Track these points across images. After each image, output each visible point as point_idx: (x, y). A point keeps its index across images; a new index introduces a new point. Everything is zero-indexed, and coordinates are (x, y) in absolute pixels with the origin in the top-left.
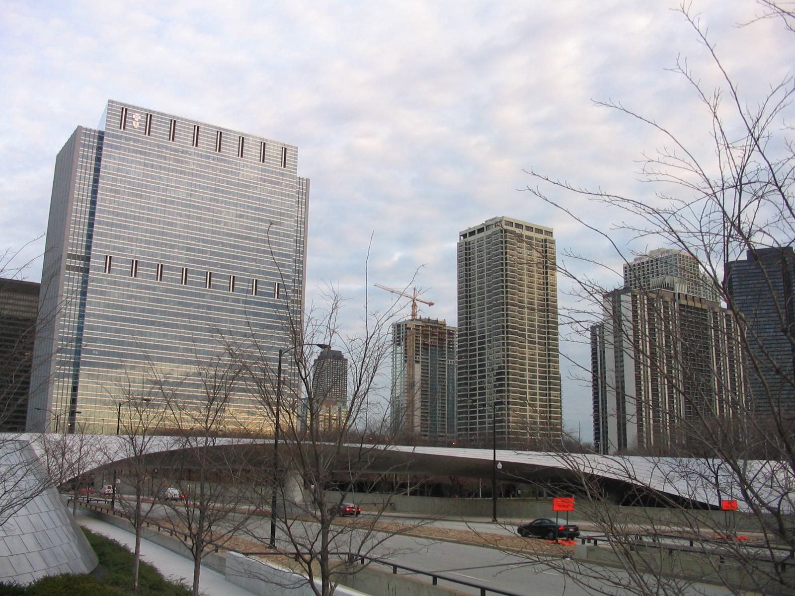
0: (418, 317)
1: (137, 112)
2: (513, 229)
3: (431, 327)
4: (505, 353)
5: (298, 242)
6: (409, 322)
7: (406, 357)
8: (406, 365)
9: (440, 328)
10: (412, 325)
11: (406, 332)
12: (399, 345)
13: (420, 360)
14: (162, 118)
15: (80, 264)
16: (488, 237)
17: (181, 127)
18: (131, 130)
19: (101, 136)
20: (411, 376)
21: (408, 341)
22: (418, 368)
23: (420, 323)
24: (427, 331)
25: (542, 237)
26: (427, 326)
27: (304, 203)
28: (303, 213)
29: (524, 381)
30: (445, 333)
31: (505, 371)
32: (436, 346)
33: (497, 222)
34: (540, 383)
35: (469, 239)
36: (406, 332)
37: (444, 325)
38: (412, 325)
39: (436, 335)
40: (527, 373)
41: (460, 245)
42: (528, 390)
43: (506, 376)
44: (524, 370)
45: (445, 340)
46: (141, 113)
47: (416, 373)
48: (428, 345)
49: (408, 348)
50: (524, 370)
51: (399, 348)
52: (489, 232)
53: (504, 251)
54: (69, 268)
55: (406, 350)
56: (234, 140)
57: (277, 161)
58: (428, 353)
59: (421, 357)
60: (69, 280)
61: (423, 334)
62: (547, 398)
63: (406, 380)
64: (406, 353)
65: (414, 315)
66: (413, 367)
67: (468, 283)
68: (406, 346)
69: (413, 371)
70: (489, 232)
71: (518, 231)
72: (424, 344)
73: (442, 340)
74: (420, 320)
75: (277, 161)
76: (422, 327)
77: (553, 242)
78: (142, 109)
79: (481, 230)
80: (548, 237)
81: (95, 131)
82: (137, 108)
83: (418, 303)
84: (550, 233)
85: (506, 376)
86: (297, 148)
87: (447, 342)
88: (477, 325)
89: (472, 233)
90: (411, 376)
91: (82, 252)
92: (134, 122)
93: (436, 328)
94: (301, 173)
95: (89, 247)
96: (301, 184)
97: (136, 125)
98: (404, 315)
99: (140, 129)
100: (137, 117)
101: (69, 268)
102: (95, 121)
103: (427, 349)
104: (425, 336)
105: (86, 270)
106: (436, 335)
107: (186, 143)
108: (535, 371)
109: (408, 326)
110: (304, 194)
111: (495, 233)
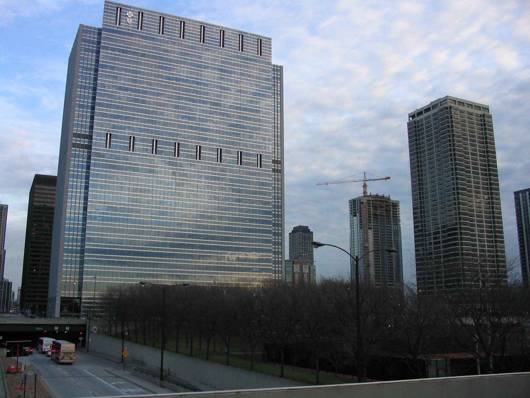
0: (368, 194)
1: (130, 10)
2: (457, 106)
3: (380, 201)
4: (457, 211)
5: (276, 180)
6: (363, 198)
7: (361, 225)
8: (361, 231)
9: (386, 202)
10: (364, 200)
11: (360, 205)
12: (355, 216)
13: (372, 227)
14: (152, 15)
15: (86, 142)
16: (434, 115)
17: (169, 22)
18: (125, 26)
19: (100, 30)
20: (365, 240)
21: (362, 212)
22: (371, 233)
23: (372, 199)
24: (376, 204)
25: (481, 112)
26: (376, 201)
27: (279, 137)
28: (280, 154)
29: (474, 235)
30: (390, 205)
31: (458, 226)
32: (383, 216)
33: (446, 99)
34: (488, 236)
35: (417, 119)
36: (360, 205)
37: (389, 199)
38: (364, 200)
39: (383, 207)
40: (476, 228)
41: (409, 124)
42: (477, 243)
43: (458, 231)
44: (473, 225)
45: (390, 211)
46: (133, 11)
47: (369, 237)
48: (378, 214)
49: (362, 217)
50: (473, 225)
51: (355, 218)
52: (436, 110)
53: (450, 125)
54: (74, 145)
55: (361, 219)
56: (216, 33)
57: (254, 50)
58: (377, 221)
59: (372, 224)
60: (75, 156)
61: (373, 207)
62: (494, 249)
63: (362, 242)
64: (361, 222)
65: (365, 192)
66: (367, 233)
67: (419, 155)
68: (361, 216)
69: (367, 235)
70: (436, 110)
71: (461, 108)
72: (374, 214)
73: (388, 211)
74: (370, 196)
75: (254, 50)
76: (373, 201)
77: (490, 117)
78: (134, 8)
79: (427, 110)
80: (486, 113)
81: (95, 29)
82: (130, 7)
83: (367, 183)
84: (487, 109)
85: (458, 231)
86: (271, 39)
87: (392, 212)
88: (429, 189)
89: (420, 113)
90: (365, 240)
91: (86, 131)
92: (128, 19)
93: (383, 201)
94: (275, 61)
95: (91, 127)
96: (276, 127)
97: (130, 21)
98: (357, 192)
99: (133, 24)
100: (130, 14)
101: (74, 145)
102: (96, 21)
103: (377, 218)
104: (375, 208)
105: (89, 147)
106: (383, 207)
107: (175, 36)
108: (482, 226)
109: (362, 201)
110: (279, 145)
111: (441, 110)
